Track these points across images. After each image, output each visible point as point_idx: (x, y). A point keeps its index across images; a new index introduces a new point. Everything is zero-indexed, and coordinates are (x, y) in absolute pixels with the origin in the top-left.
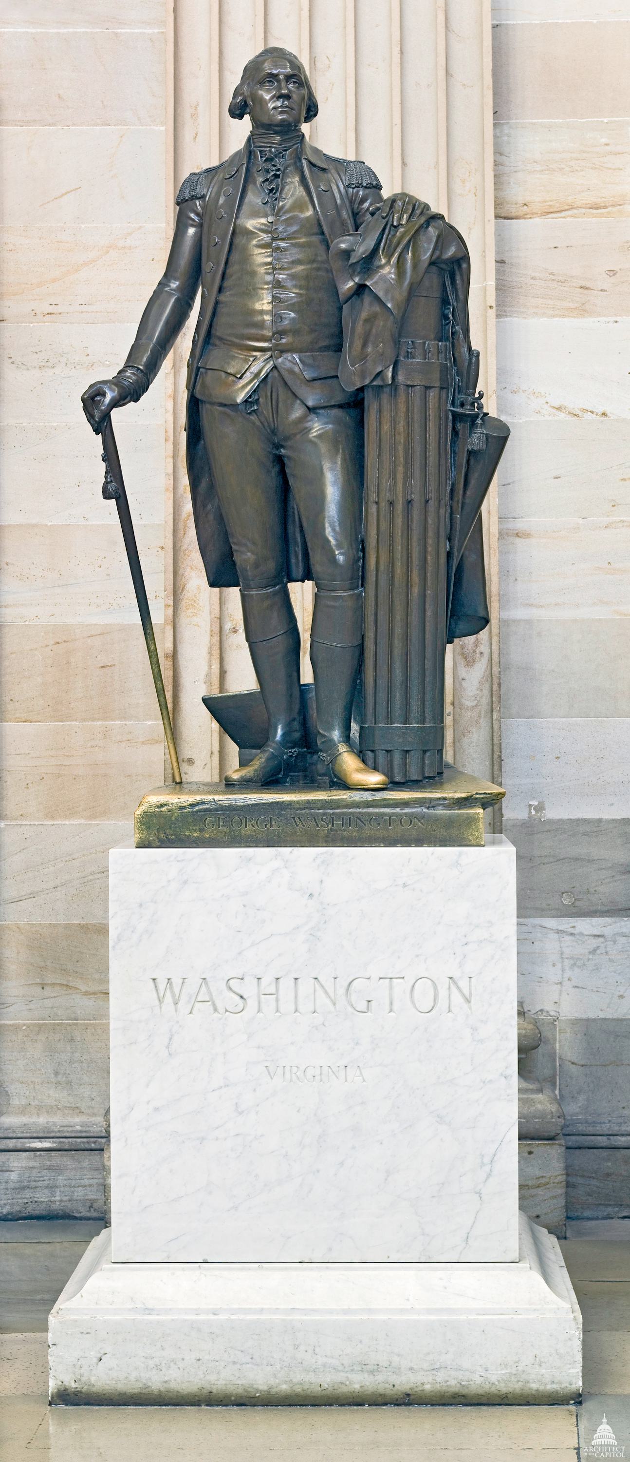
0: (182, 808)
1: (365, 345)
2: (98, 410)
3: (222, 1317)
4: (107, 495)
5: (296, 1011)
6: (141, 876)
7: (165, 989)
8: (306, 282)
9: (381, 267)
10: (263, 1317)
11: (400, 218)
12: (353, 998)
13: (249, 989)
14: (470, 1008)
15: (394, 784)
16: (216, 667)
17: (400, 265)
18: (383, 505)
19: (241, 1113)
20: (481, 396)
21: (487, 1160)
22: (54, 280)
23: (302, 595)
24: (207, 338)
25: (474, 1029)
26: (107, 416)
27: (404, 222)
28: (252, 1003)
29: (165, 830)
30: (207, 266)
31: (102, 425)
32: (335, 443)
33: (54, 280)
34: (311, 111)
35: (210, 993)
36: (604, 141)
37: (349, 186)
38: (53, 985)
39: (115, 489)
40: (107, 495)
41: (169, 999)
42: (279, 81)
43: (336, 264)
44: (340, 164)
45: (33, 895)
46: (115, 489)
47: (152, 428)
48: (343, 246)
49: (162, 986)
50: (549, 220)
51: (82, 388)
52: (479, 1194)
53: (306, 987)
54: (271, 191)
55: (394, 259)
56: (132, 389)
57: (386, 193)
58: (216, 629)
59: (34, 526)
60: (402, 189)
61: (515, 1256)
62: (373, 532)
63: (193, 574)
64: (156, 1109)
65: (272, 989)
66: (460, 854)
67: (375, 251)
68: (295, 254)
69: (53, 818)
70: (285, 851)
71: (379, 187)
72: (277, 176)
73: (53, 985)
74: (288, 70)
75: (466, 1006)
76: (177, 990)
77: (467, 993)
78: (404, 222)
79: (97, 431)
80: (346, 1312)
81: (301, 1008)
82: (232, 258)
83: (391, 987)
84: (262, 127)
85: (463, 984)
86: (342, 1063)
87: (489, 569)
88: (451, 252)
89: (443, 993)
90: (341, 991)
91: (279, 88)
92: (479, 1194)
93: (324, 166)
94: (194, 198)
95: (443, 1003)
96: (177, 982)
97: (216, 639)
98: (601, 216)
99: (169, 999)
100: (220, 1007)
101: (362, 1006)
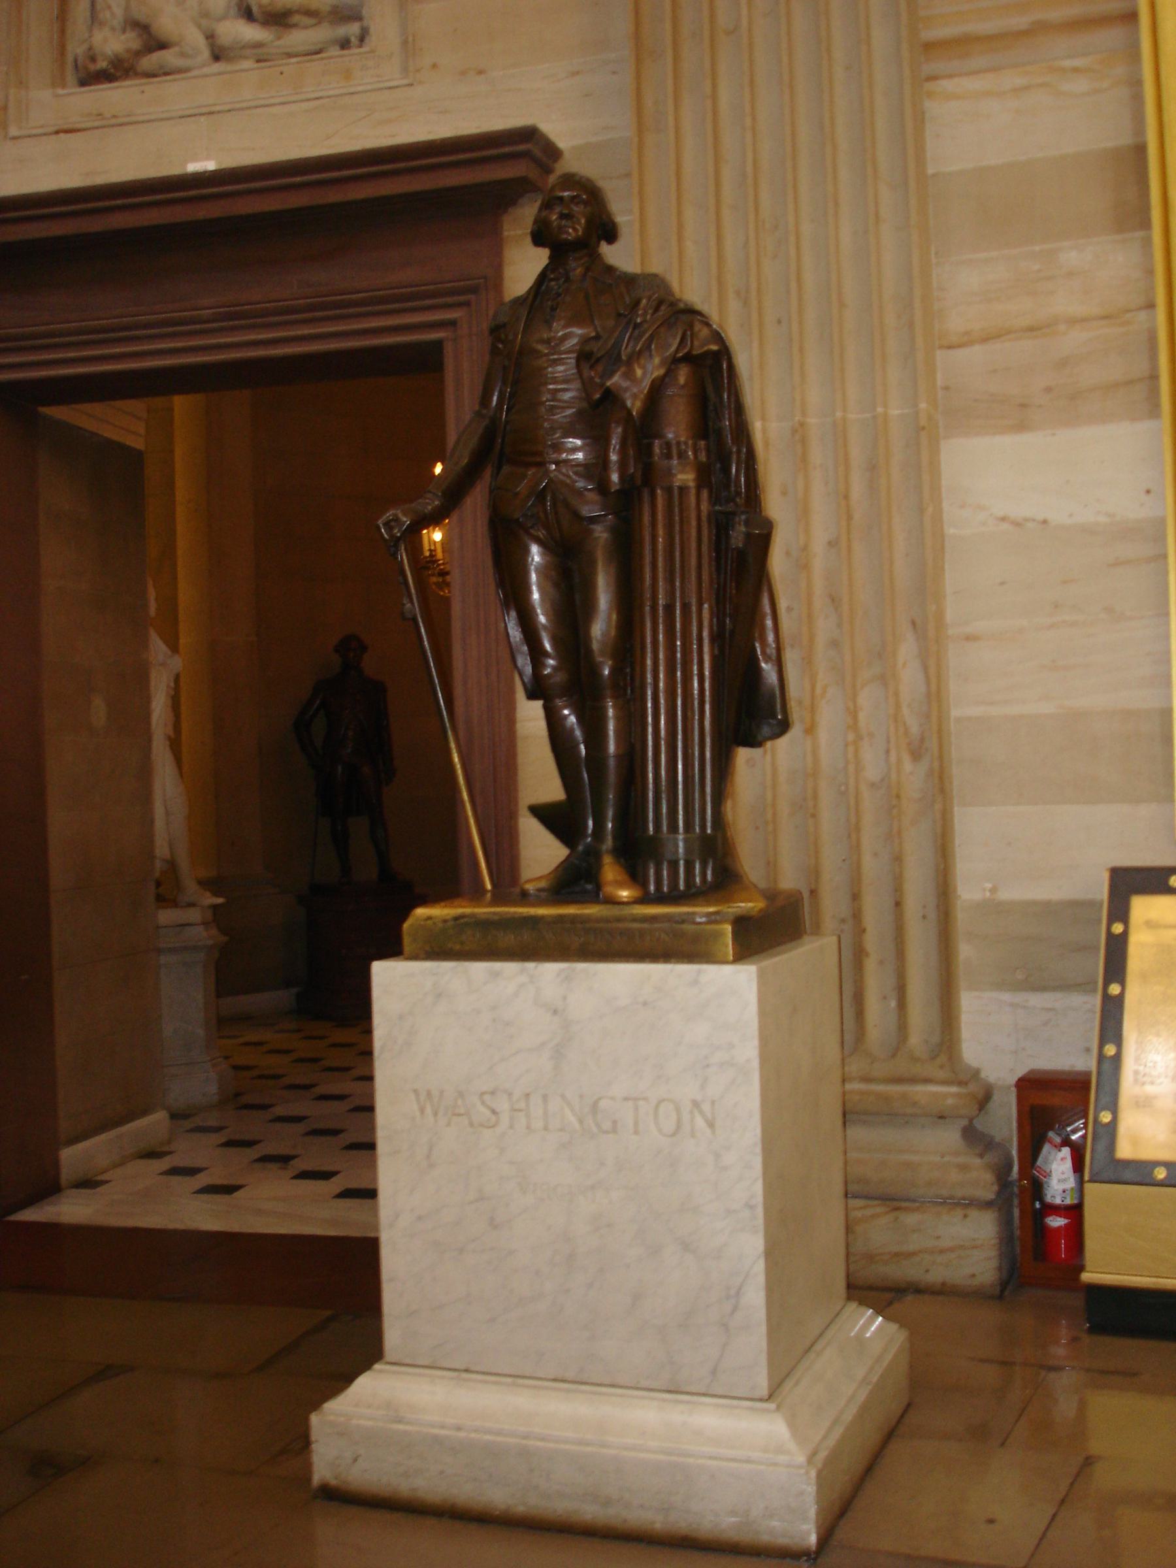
0: (445, 921)
3: (462, 1434)
10: (500, 1439)
13: (503, 1105)
14: (436, 1121)
15: (645, 899)
21: (732, 1292)
28: (505, 1119)
36: (1036, 267)
41: (429, 1110)
49: (422, 1098)
61: (764, 1392)
64: (420, 1218)
66: (699, 972)
70: (530, 965)
75: (708, 1131)
77: (709, 1115)
80: (581, 1443)
83: (636, 1109)
85: (706, 1107)
87: (183, 79)
99: (429, 1110)
101: (607, 1125)
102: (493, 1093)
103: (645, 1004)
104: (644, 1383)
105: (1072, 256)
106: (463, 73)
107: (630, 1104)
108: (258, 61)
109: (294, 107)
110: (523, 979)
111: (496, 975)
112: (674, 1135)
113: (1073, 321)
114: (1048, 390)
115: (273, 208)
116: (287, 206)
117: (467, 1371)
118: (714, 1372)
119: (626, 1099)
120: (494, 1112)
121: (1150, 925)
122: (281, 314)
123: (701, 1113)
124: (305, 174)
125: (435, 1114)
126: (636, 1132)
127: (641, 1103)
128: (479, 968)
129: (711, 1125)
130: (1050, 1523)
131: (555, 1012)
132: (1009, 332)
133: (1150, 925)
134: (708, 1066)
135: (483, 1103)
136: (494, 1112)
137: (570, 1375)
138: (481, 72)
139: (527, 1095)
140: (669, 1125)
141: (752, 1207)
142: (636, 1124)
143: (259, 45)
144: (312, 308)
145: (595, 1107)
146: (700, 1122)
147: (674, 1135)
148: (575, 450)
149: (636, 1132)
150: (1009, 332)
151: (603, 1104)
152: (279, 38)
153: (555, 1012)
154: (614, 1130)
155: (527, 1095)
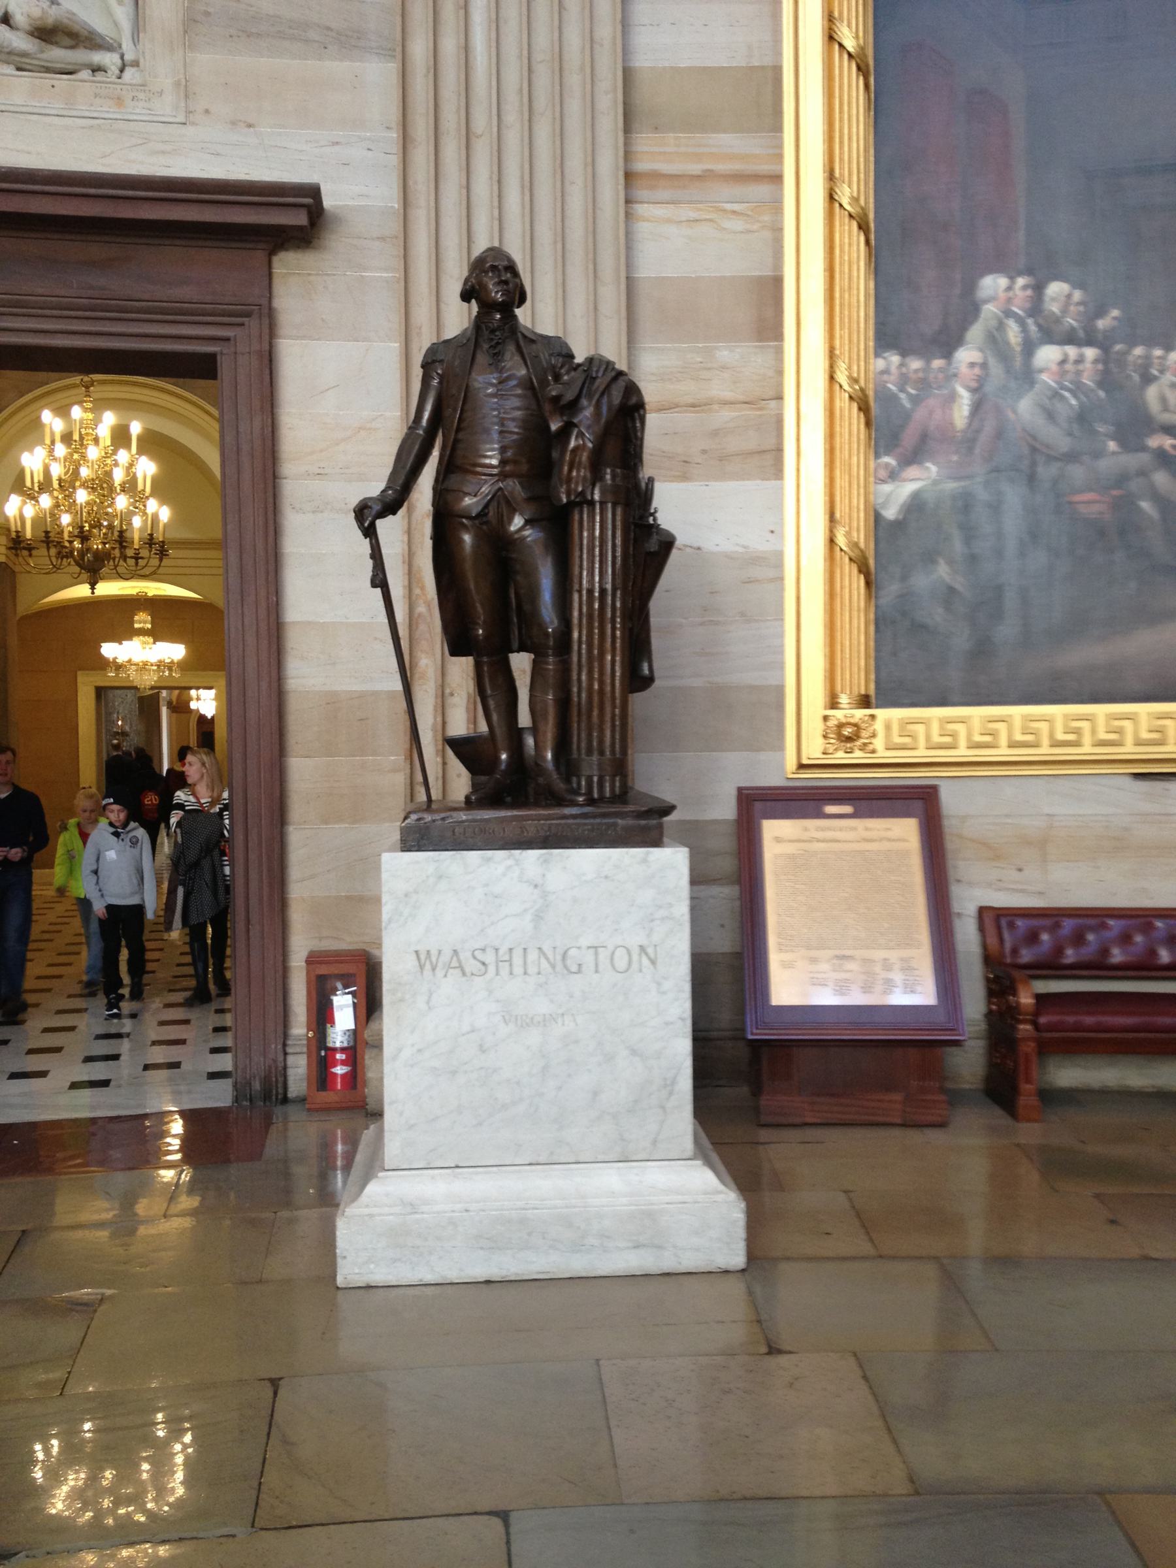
1: (570, 471)
2: (367, 517)
4: (374, 585)
5: (525, 973)
6: (403, 872)
7: (424, 960)
8: (525, 424)
9: (583, 408)
11: (597, 371)
12: (569, 962)
13: (489, 958)
16: (439, 719)
17: (598, 406)
18: (584, 592)
19: (484, 1052)
20: (656, 512)
22: (321, 451)
23: (521, 663)
24: (447, 469)
25: (659, 984)
26: (373, 525)
27: (600, 374)
28: (492, 969)
29: (418, 838)
30: (448, 412)
31: (370, 532)
32: (546, 547)
33: (321, 451)
34: (522, 299)
35: (459, 961)
36: (699, 359)
37: (551, 355)
38: (327, 937)
39: (380, 580)
40: (374, 585)
41: (428, 967)
42: (499, 271)
43: (547, 407)
44: (546, 339)
45: (312, 877)
46: (380, 580)
47: (408, 536)
48: (554, 393)
49: (423, 957)
50: (662, 415)
51: (354, 501)
52: (663, 1107)
53: (533, 956)
54: (495, 354)
55: (594, 402)
56: (393, 501)
57: (579, 359)
58: (440, 693)
59: (309, 623)
60: (596, 348)
62: (576, 614)
63: (423, 656)
64: (419, 1051)
65: (507, 958)
66: (648, 853)
67: (578, 397)
68: (516, 402)
69: (326, 823)
71: (572, 357)
72: (498, 343)
73: (327, 937)
74: (506, 263)
76: (434, 959)
77: (652, 956)
78: (600, 374)
79: (366, 536)
81: (529, 971)
82: (466, 408)
83: (596, 954)
84: (487, 307)
85: (650, 951)
86: (560, 1011)
88: (634, 400)
89: (635, 957)
90: (559, 958)
91: (499, 276)
92: (663, 1107)
93: (533, 339)
94: (434, 362)
95: (635, 966)
96: (434, 953)
97: (439, 700)
98: (697, 412)
99: (428, 967)
100: (468, 970)
101: (574, 968)
102: (483, 950)
103: (606, 877)
104: (600, 1158)
105: (725, 354)
106: (233, 123)
107: (592, 951)
108: (19, 69)
109: (69, 121)
110: (510, 862)
111: (489, 860)
112: (626, 971)
113: (726, 403)
114: (704, 452)
115: (65, 212)
116: (81, 213)
117: (457, 1167)
118: (654, 1142)
119: (589, 947)
120: (484, 964)
121: (778, 840)
122: (145, 313)
123: (647, 954)
124: (46, 185)
125: (434, 969)
126: (597, 971)
127: (600, 950)
128: (473, 856)
129: (653, 962)
130: (273, 1406)
131: (536, 886)
132: (677, 406)
133: (778, 840)
134: (652, 921)
135: (475, 958)
136: (484, 964)
137: (542, 1159)
138: (250, 126)
139: (511, 950)
140: (621, 963)
141: (683, 1019)
142: (597, 965)
143: (24, 54)
144: (92, 309)
145: (564, 956)
146: (645, 961)
147: (626, 971)
148: (490, 457)
149: (597, 971)
150: (677, 406)
151: (572, 952)
152: (42, 52)
153: (536, 886)
154: (579, 972)
155: (511, 950)
